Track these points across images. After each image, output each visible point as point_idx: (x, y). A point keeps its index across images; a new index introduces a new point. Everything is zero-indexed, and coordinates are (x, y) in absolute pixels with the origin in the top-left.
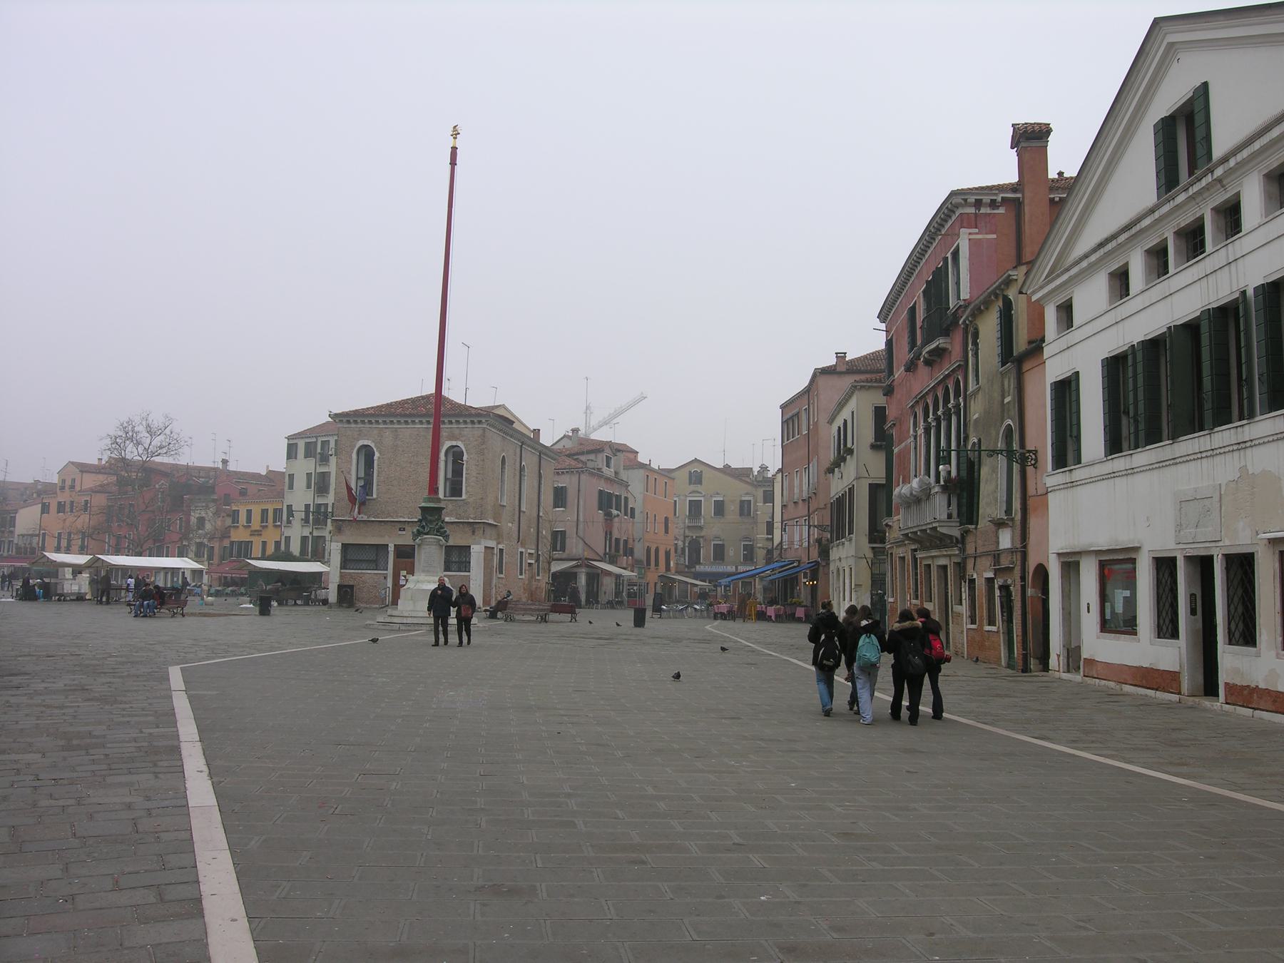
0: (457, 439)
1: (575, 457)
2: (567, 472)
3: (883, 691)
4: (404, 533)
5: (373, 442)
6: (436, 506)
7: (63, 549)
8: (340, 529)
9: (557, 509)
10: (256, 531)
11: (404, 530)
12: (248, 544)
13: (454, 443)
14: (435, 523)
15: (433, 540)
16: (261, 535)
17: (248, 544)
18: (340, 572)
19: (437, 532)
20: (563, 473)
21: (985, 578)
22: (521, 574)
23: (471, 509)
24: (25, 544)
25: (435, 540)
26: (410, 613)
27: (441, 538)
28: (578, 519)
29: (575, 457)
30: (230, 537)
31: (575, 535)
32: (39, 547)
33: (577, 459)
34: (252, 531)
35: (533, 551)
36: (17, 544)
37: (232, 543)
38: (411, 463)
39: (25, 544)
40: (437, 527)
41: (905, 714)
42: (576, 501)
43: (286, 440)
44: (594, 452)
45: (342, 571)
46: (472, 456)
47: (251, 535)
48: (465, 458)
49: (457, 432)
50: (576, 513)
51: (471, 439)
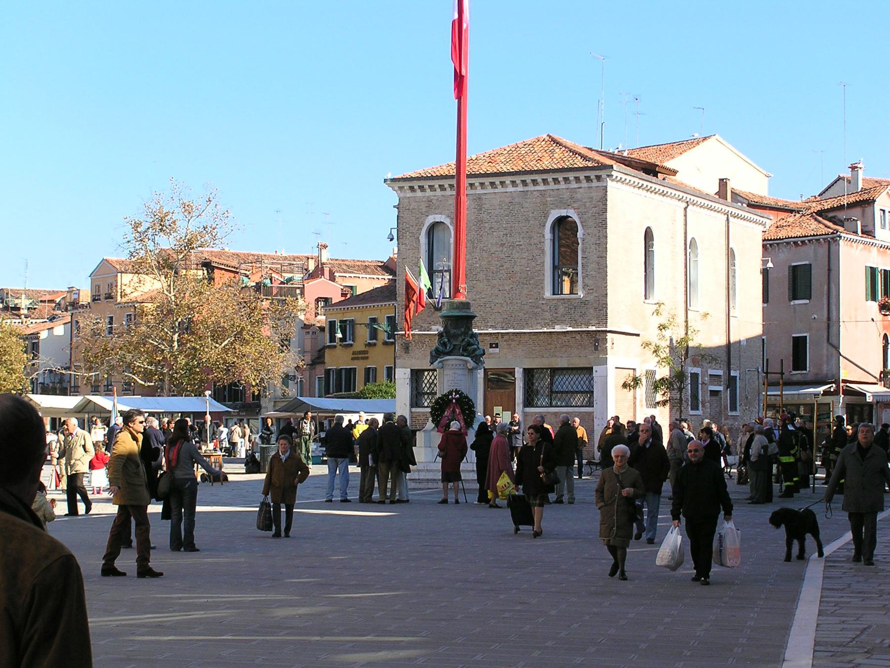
0: (567, 206)
1: (831, 215)
2: (809, 241)
3: (283, 508)
4: (497, 350)
5: (448, 216)
6: (460, 314)
7: (102, 389)
8: (408, 348)
9: (797, 302)
10: (360, 352)
11: (497, 347)
12: (351, 372)
13: (563, 213)
14: (460, 339)
15: (457, 362)
16: (367, 358)
17: (351, 372)
18: (411, 412)
19: (465, 350)
20: (803, 242)
21: (710, 391)
22: (734, 408)
23: (591, 311)
24: (54, 383)
25: (460, 362)
26: (425, 465)
27: (469, 359)
28: (829, 319)
29: (831, 215)
30: (324, 363)
31: (826, 341)
32: (71, 387)
33: (834, 217)
34: (354, 353)
35: (720, 372)
36: (43, 384)
37: (328, 372)
38: (502, 245)
39: (54, 383)
40: (464, 344)
41: (283, 534)
42: (826, 288)
43: (850, 169)
44: (861, 206)
45: (414, 410)
46: (590, 231)
47: (353, 359)
48: (580, 234)
49: (566, 195)
50: (826, 307)
51: (588, 204)
